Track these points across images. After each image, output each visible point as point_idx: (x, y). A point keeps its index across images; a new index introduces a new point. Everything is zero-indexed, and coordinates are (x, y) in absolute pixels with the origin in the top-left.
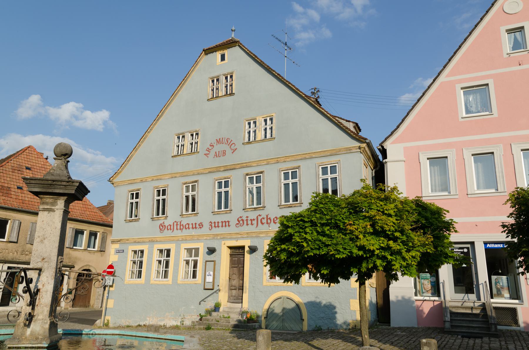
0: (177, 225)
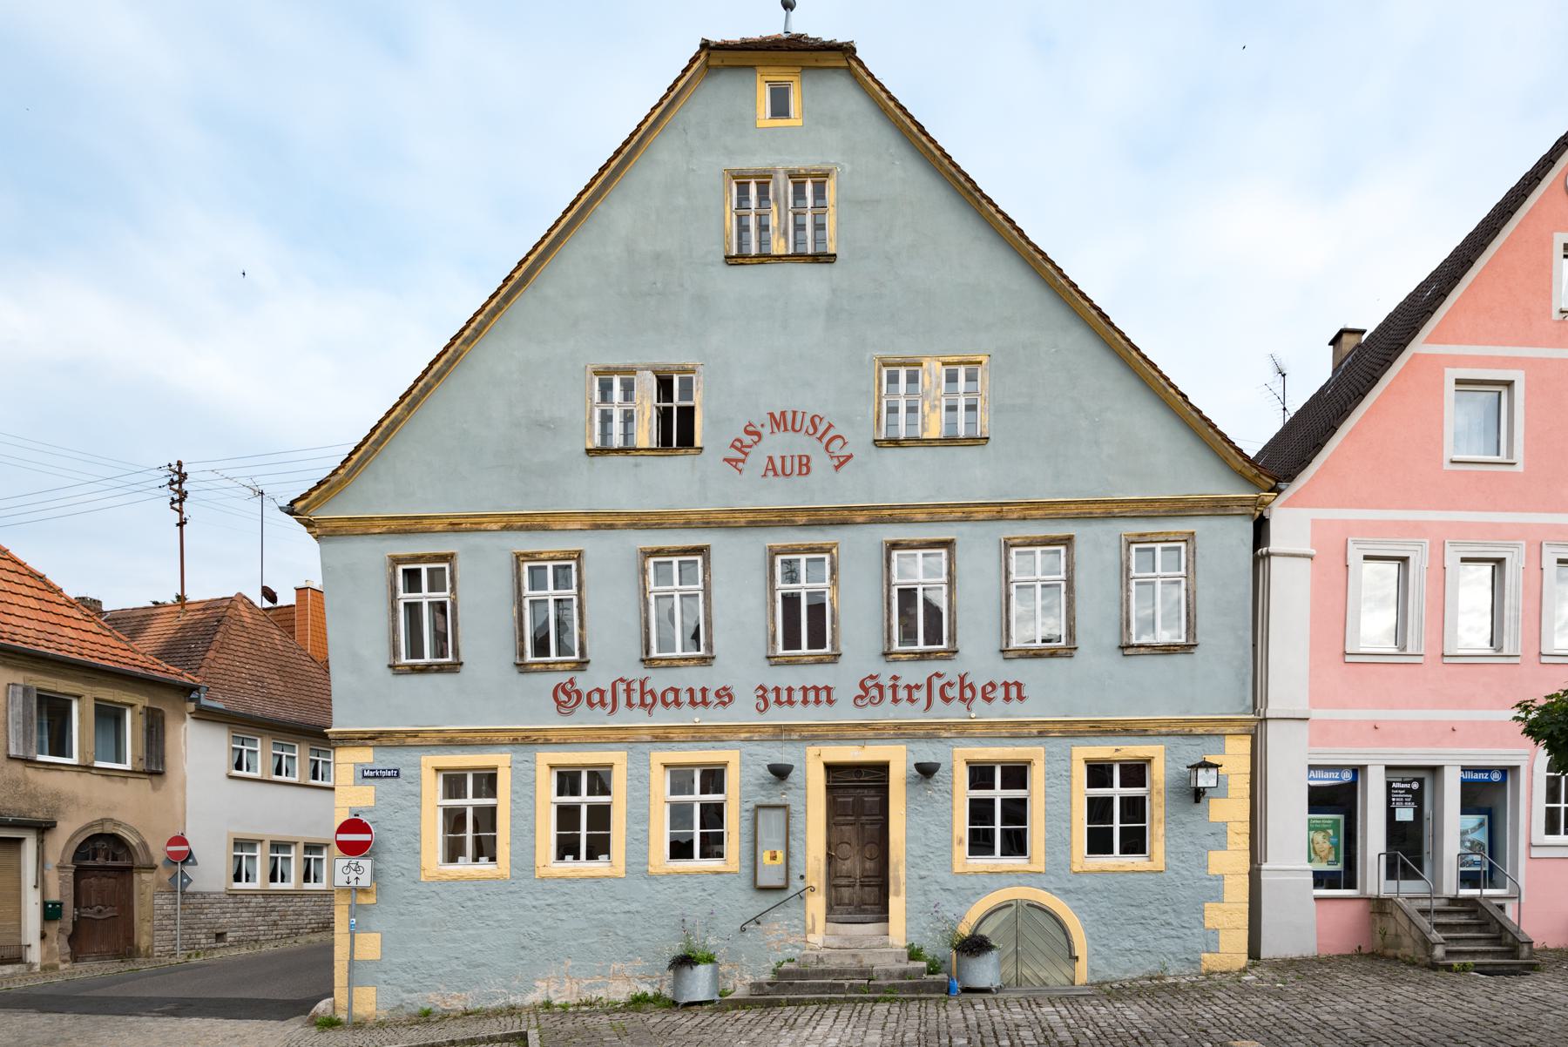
0: (629, 691)
